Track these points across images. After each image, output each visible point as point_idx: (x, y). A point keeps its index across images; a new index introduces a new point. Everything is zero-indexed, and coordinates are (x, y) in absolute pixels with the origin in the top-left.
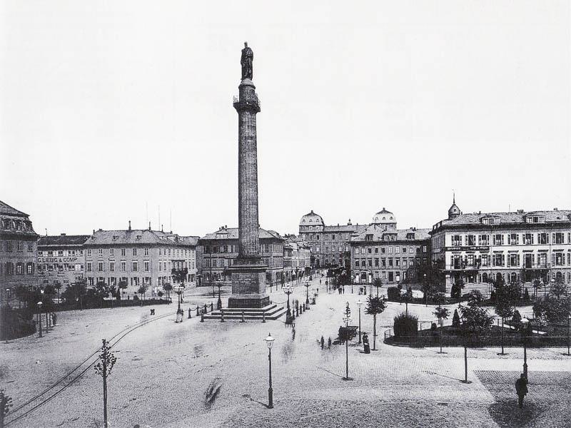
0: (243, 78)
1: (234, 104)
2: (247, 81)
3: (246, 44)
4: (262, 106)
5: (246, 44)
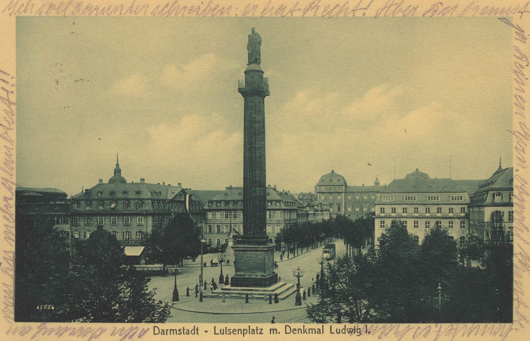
0: (250, 63)
1: (239, 89)
2: (254, 66)
4: (271, 89)
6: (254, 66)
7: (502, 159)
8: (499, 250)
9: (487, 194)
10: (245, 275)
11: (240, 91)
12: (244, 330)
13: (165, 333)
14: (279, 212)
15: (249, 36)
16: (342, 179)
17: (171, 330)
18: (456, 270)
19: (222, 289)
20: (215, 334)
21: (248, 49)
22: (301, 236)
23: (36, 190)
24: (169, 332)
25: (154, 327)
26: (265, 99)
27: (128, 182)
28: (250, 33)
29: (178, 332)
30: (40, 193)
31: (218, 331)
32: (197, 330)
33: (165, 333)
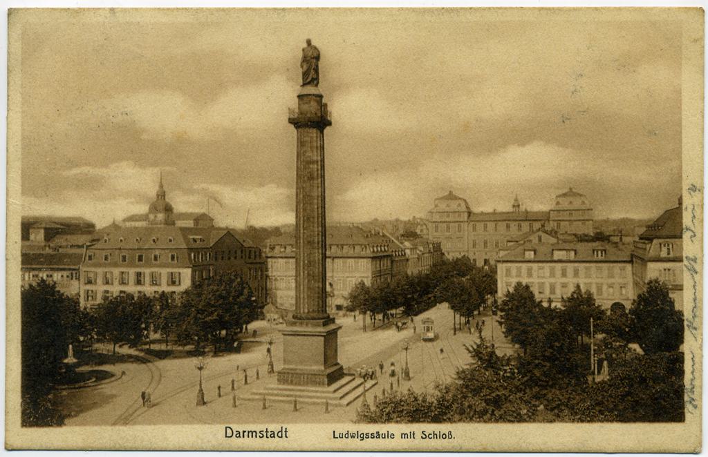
1: (289, 119)
2: (310, 90)
3: (309, 42)
5: (309, 42)
6: (310, 90)
7: (260, 372)
8: (658, 323)
9: (651, 243)
10: (296, 369)
11: (291, 121)
12: (282, 437)
13: (241, 435)
14: (365, 260)
15: (303, 50)
16: (463, 204)
17: (249, 432)
18: (609, 352)
19: (266, 389)
20: (334, 437)
21: (302, 67)
22: (396, 297)
23: (56, 221)
24: (246, 434)
25: (226, 428)
26: (325, 131)
27: (175, 211)
28: (305, 45)
29: (258, 435)
30: (62, 224)
31: (337, 435)
32: (286, 432)
33: (241, 435)
